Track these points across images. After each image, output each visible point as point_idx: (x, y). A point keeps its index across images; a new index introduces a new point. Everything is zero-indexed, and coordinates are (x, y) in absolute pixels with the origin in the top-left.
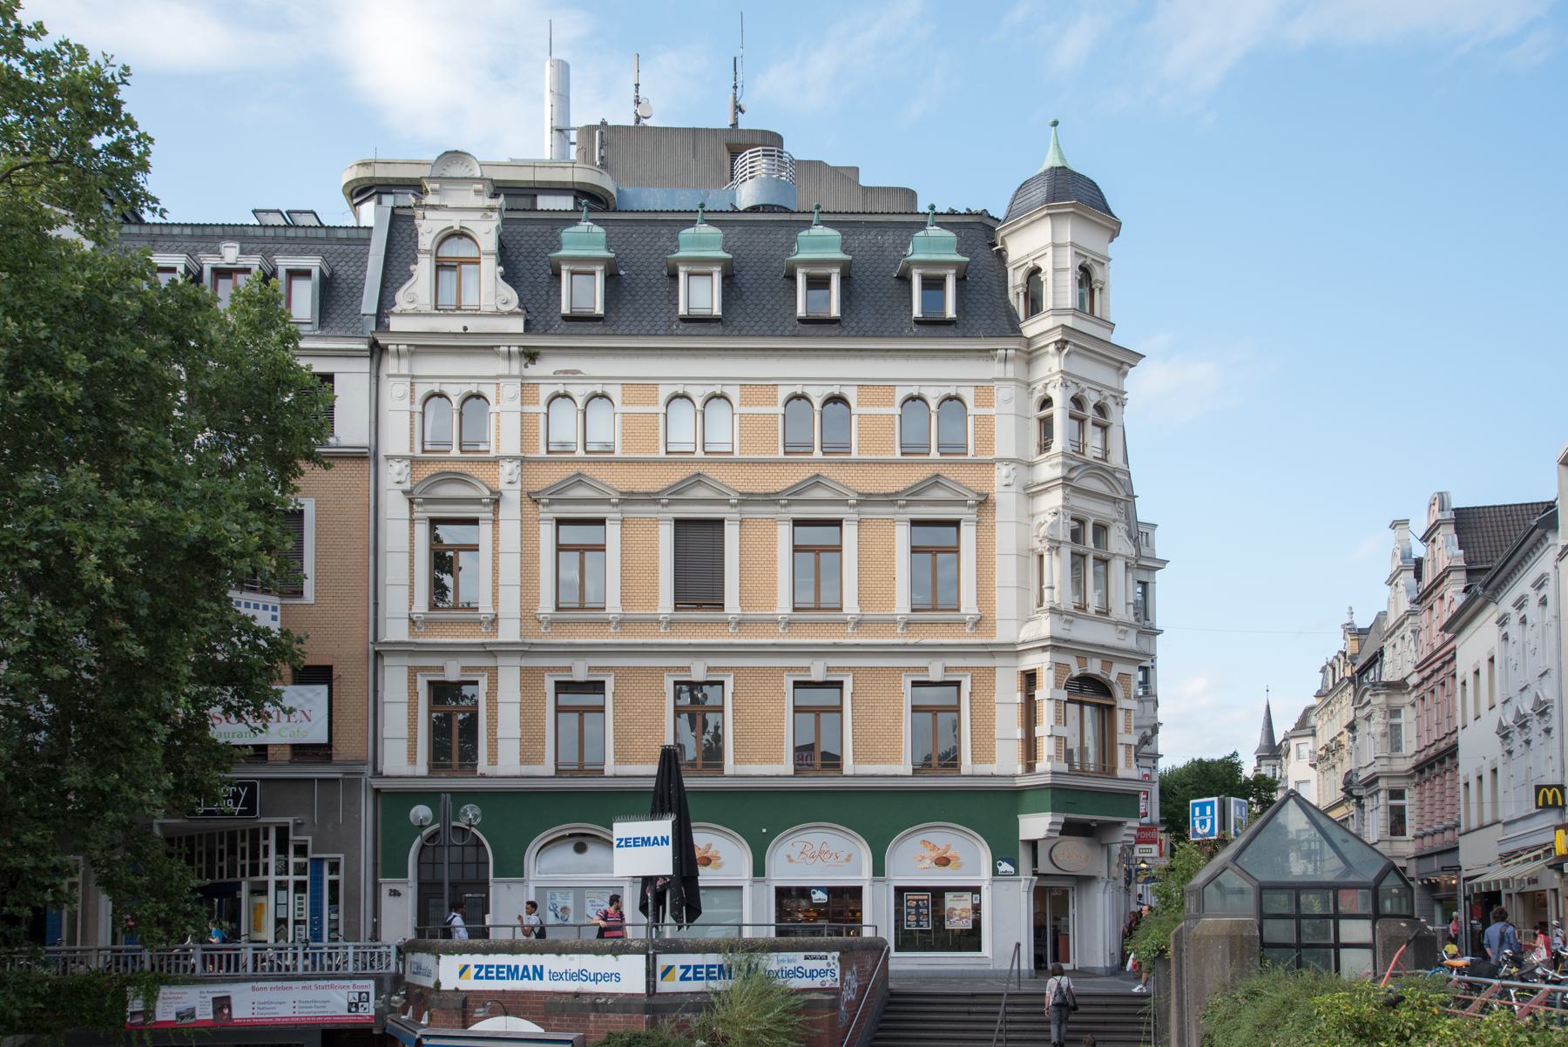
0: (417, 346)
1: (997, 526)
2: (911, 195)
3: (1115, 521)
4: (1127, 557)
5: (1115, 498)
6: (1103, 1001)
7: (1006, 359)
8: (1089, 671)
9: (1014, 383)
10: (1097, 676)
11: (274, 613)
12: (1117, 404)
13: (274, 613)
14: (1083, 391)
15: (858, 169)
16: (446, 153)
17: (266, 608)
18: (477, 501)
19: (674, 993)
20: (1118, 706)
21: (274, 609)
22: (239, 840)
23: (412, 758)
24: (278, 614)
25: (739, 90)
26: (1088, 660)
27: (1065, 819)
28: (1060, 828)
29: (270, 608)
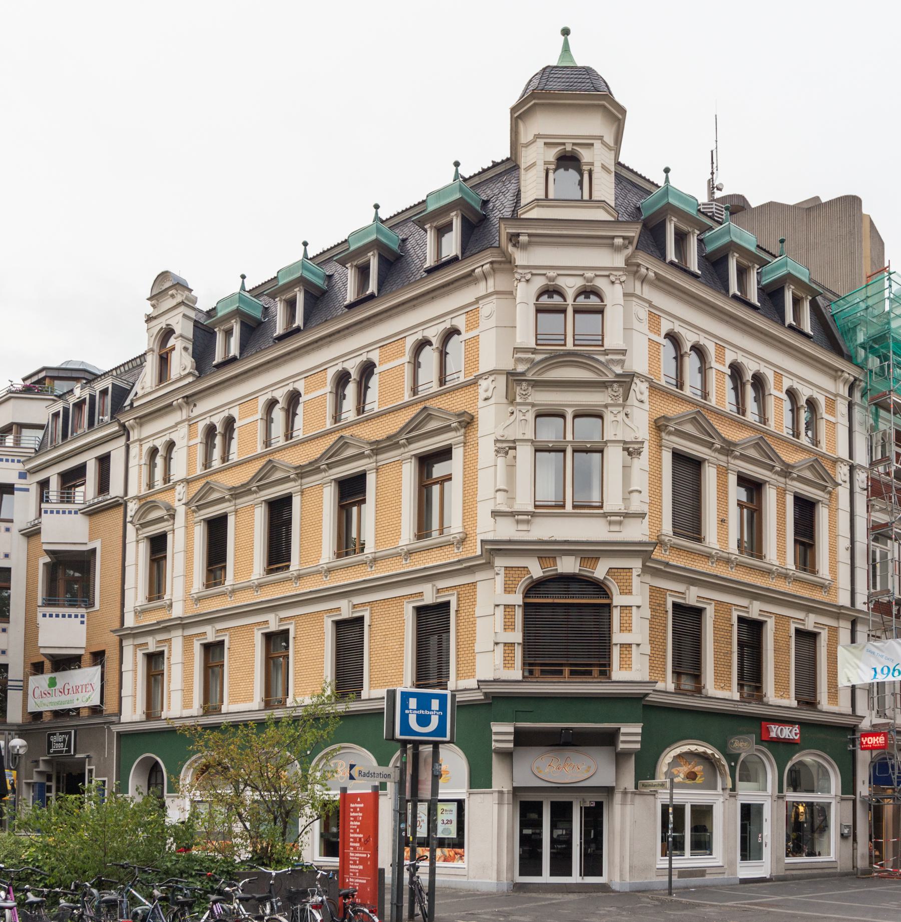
0: (140, 418)
1: (480, 441)
2: (817, 198)
3: (606, 406)
4: (625, 442)
5: (604, 382)
6: (807, 872)
7: (485, 277)
8: (560, 571)
9: (495, 297)
10: (544, 577)
11: (82, 619)
12: (613, 283)
13: (82, 619)
14: (552, 279)
15: (852, 203)
16: (158, 276)
17: (76, 616)
18: (160, 520)
19: (724, 817)
20: (614, 604)
21: (83, 616)
22: (87, 764)
23: (187, 704)
24: (85, 619)
25: (714, 175)
26: (558, 560)
27: (515, 728)
28: (511, 738)
29: (79, 616)
